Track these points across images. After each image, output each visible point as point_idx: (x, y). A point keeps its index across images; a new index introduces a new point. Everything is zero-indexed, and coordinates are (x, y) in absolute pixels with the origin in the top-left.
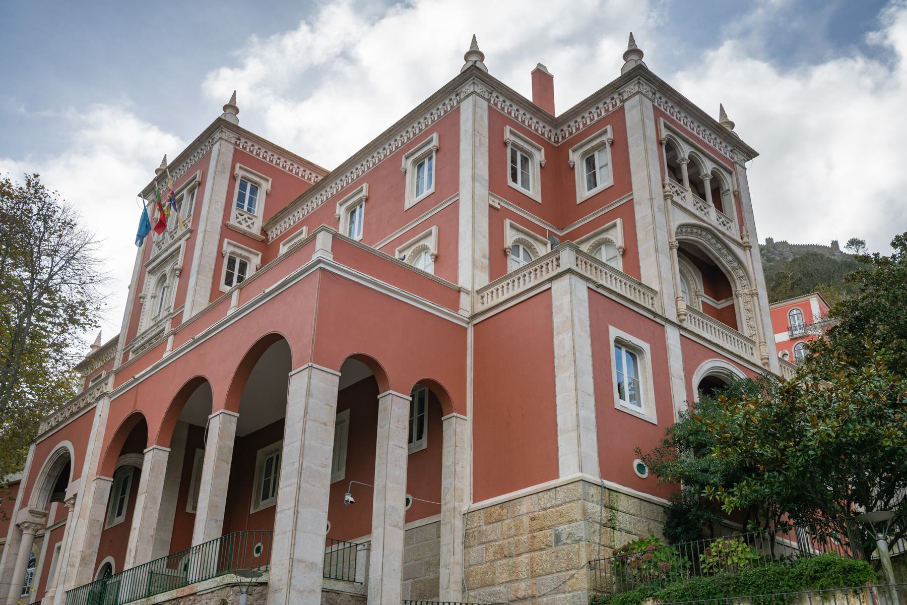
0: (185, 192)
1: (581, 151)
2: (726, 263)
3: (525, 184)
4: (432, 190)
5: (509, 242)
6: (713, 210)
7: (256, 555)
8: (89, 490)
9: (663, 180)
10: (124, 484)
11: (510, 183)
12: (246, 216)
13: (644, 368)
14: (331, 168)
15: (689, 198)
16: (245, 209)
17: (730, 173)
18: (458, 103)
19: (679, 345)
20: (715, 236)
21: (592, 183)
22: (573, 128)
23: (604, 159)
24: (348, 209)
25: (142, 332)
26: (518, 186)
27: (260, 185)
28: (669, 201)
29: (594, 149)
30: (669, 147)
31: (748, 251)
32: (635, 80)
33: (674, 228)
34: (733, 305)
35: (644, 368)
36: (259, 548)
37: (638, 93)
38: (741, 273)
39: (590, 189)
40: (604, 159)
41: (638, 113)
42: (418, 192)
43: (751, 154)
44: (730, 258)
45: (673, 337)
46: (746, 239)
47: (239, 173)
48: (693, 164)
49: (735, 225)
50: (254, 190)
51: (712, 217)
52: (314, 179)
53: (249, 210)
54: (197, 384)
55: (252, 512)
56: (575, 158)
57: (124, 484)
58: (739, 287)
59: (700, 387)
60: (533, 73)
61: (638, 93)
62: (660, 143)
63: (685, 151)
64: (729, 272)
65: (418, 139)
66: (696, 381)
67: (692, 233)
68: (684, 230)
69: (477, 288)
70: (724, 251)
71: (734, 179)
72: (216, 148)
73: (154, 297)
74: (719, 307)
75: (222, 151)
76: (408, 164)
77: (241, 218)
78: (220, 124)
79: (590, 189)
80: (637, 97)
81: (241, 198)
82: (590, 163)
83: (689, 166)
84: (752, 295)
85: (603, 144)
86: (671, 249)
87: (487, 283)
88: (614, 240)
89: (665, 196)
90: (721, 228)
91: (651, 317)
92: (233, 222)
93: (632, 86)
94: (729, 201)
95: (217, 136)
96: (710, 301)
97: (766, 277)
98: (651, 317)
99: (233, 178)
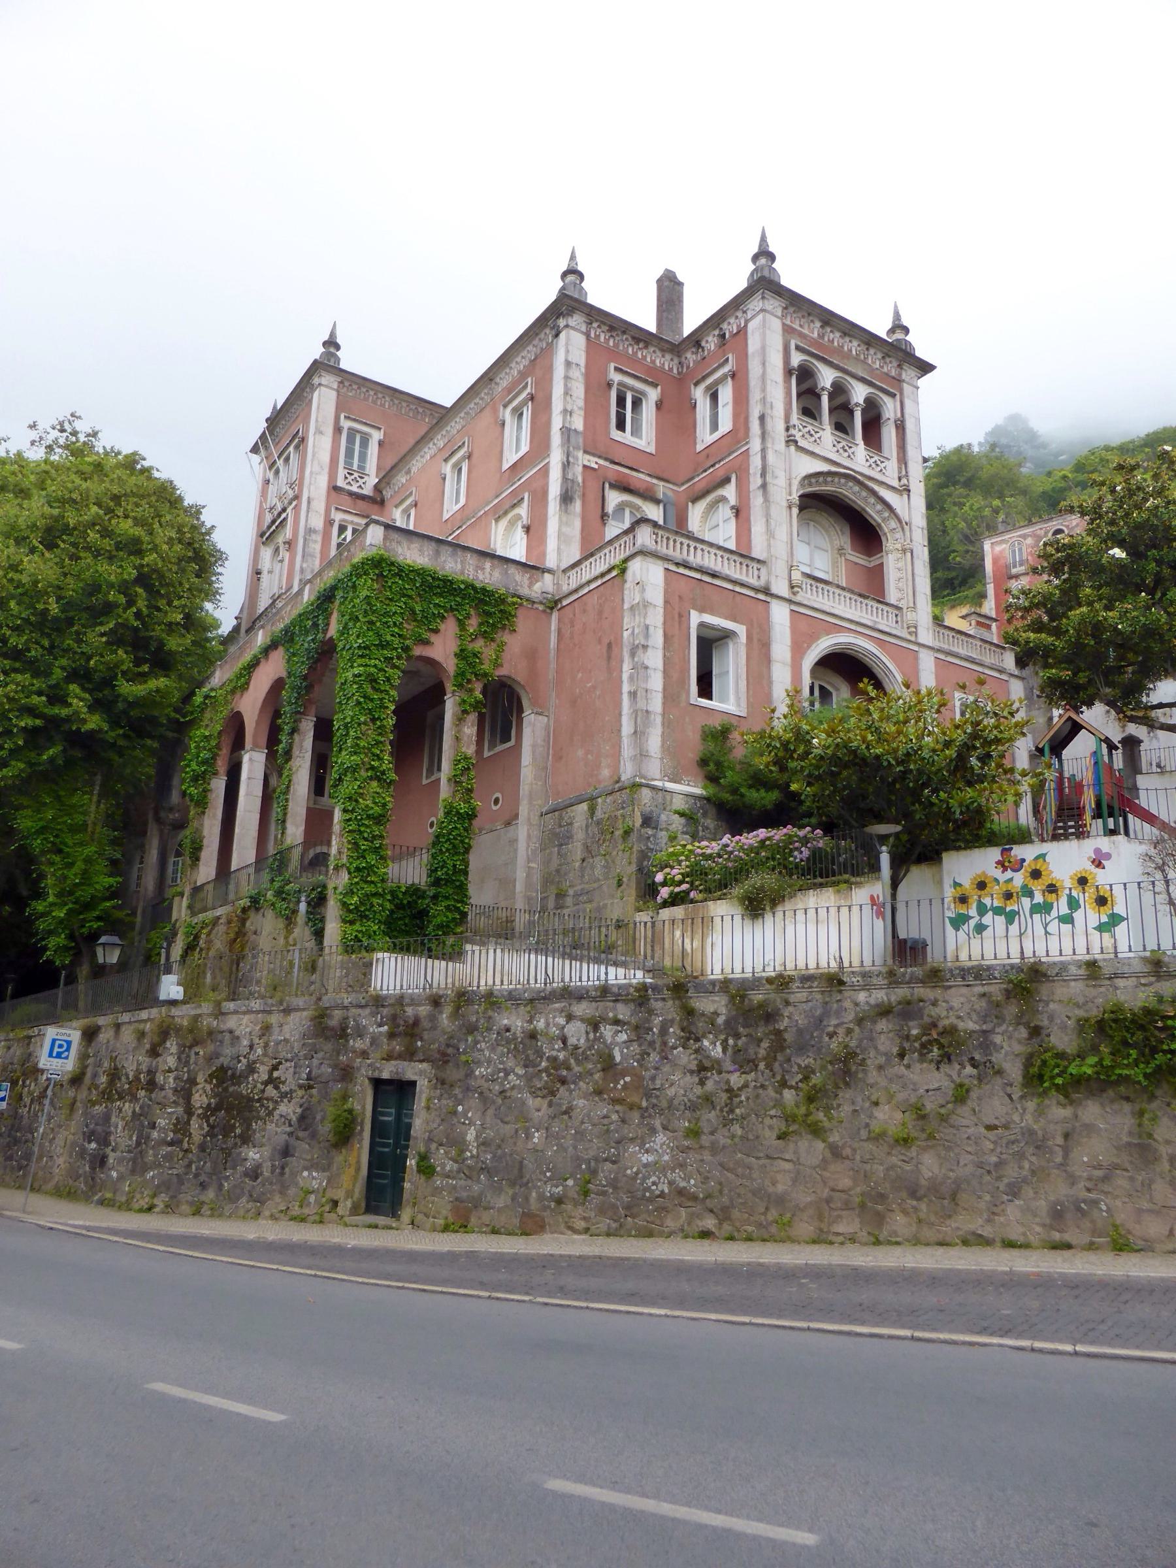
0: (291, 449)
1: (703, 386)
2: (873, 512)
3: (636, 432)
4: (525, 448)
5: (610, 507)
6: (860, 449)
7: (494, 808)
8: (253, 764)
10: (277, 760)
11: (616, 435)
12: (356, 475)
13: (737, 654)
14: (449, 405)
15: (826, 438)
16: (355, 467)
17: (893, 396)
18: (747, 322)
19: (788, 623)
21: (715, 426)
23: (726, 394)
24: (454, 466)
25: (262, 609)
26: (626, 437)
27: (370, 435)
28: (793, 448)
30: (805, 375)
31: (905, 496)
32: (759, 295)
33: (795, 484)
34: (882, 565)
35: (737, 654)
37: (762, 310)
38: (893, 524)
39: (711, 433)
40: (726, 394)
41: (766, 334)
42: (518, 449)
43: (925, 368)
44: (879, 507)
45: (780, 615)
46: (904, 481)
47: (346, 424)
48: (838, 390)
51: (859, 458)
52: (444, 412)
55: (425, 782)
57: (277, 760)
58: (891, 542)
59: (449, 780)
60: (659, 281)
61: (762, 310)
62: (789, 372)
63: (826, 377)
64: (879, 525)
65: (515, 384)
67: (826, 483)
68: (813, 480)
69: (564, 565)
70: (872, 500)
71: (898, 404)
72: (316, 394)
73: (270, 572)
74: (872, 564)
75: (324, 400)
77: (350, 478)
78: (316, 367)
79: (711, 433)
80: (761, 316)
81: (349, 453)
82: (714, 397)
83: (832, 397)
84: (904, 551)
85: (724, 377)
86: (790, 507)
87: (578, 557)
88: (727, 495)
89: (787, 442)
92: (340, 483)
93: (755, 303)
94: (889, 434)
95: (316, 381)
96: (860, 559)
99: (338, 430)
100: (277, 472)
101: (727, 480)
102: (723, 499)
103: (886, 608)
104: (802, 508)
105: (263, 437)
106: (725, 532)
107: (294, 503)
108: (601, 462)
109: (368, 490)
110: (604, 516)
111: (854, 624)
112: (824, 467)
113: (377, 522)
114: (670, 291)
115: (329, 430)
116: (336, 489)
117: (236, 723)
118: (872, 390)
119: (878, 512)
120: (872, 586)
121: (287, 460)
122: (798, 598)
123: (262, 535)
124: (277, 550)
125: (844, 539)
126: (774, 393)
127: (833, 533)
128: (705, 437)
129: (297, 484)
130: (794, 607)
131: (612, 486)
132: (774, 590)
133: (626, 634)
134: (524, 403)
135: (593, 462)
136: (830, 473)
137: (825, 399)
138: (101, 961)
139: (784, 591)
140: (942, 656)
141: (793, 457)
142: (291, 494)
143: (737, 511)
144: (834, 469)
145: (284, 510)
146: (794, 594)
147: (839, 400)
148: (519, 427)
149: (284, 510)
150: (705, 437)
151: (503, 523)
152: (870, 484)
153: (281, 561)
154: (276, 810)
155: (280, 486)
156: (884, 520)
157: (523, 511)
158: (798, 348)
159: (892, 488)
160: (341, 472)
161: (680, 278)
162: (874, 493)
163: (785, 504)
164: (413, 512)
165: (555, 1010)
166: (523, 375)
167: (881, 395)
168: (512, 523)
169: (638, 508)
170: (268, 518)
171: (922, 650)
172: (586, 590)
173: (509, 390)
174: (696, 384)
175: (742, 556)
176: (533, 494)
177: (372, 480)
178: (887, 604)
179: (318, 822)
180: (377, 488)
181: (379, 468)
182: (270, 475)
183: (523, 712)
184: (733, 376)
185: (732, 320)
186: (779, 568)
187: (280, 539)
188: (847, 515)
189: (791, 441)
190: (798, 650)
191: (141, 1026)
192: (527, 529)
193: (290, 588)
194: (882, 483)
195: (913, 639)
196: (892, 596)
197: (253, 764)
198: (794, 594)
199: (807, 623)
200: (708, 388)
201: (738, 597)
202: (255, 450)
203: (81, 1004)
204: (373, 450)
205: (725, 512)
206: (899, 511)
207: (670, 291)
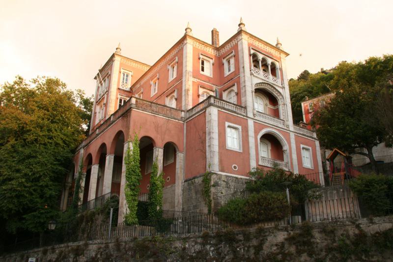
0: (106, 78)
2: (275, 94)
4: (175, 76)
6: (271, 76)
9: (250, 68)
11: (202, 72)
18: (238, 42)
20: (270, 85)
21: (229, 70)
22: (223, 51)
23: (232, 61)
29: (230, 58)
30: (254, 56)
33: (253, 86)
34: (278, 108)
36: (168, 179)
38: (281, 97)
40: (232, 61)
42: (173, 77)
44: (277, 92)
45: (251, 123)
46: (283, 85)
47: (122, 71)
48: (264, 60)
49: (279, 81)
50: (127, 76)
51: (270, 79)
53: (126, 83)
54: (103, 146)
56: (225, 61)
58: (280, 102)
62: (250, 55)
63: (260, 57)
66: (259, 137)
70: (275, 90)
73: (99, 113)
76: (170, 67)
82: (229, 62)
83: (262, 62)
85: (232, 56)
86: (252, 92)
90: (274, 83)
91: (242, 117)
94: (278, 72)
96: (272, 107)
97: (291, 95)
98: (242, 117)
100: (102, 84)
101: (234, 85)
102: (233, 90)
103: (280, 121)
104: (255, 92)
105: (98, 74)
106: (234, 100)
107: (107, 93)
108: (198, 80)
109: (128, 89)
110: (199, 96)
111: (272, 126)
112: (261, 81)
113: (134, 97)
114: (214, 33)
115: (118, 72)
116: (119, 89)
117: (90, 157)
118: (273, 60)
119: (277, 94)
120: (276, 114)
121: (105, 81)
122: (255, 118)
123: (97, 102)
124: (101, 106)
125: (267, 102)
126: (247, 61)
127: (264, 100)
128: (227, 73)
129: (109, 87)
130: (254, 121)
131: (201, 87)
132: (248, 115)
133: (207, 129)
134: (175, 64)
135: (195, 80)
136: (263, 83)
137: (260, 63)
138: (50, 228)
139: (251, 116)
140: (220, 109)
141: (252, 78)
142: (106, 91)
143: (237, 94)
144: (264, 82)
145: (104, 95)
146: (255, 117)
147: (264, 63)
148: (173, 71)
149: (104, 95)
150: (227, 73)
151: (169, 98)
152: (274, 86)
153: (103, 110)
154: (100, 181)
155: (103, 89)
156: (278, 96)
157: (175, 94)
158: (252, 49)
159: (280, 87)
160: (121, 84)
161: (218, 30)
162: (275, 88)
163: (251, 91)
164: (141, 95)
165: (191, 241)
166: (175, 56)
167: (276, 62)
168: (172, 98)
169: (208, 93)
170: (99, 97)
171: (249, 119)
172: (194, 117)
173: (170, 60)
174: (224, 58)
175: (239, 106)
176: (178, 90)
177: (129, 86)
178: (224, 101)
179: (116, 186)
180: (131, 88)
181: (132, 83)
182: (100, 85)
183: (176, 152)
184: (234, 56)
185: (233, 41)
186: (250, 109)
187: (102, 103)
188: (267, 94)
189: (251, 74)
190: (256, 133)
191: (62, 249)
192: (176, 99)
193: (105, 117)
194: (277, 86)
195: (245, 114)
196: (282, 117)
197: (95, 169)
198: (255, 117)
199: (258, 126)
200: (227, 60)
201: (239, 118)
202: (95, 78)
203: (41, 242)
204: (130, 77)
205: (233, 94)
206: (282, 93)
207: (214, 33)
